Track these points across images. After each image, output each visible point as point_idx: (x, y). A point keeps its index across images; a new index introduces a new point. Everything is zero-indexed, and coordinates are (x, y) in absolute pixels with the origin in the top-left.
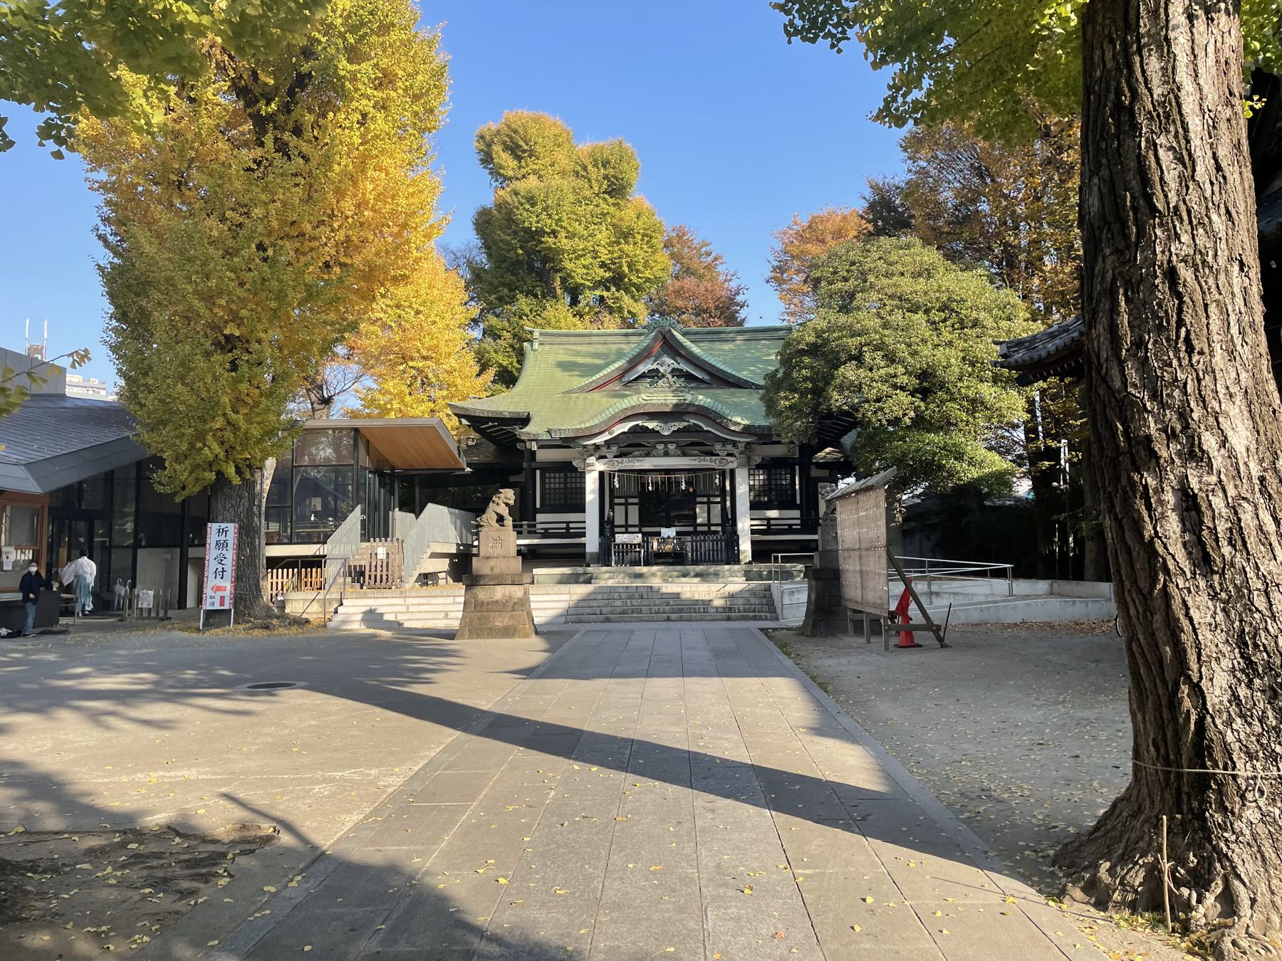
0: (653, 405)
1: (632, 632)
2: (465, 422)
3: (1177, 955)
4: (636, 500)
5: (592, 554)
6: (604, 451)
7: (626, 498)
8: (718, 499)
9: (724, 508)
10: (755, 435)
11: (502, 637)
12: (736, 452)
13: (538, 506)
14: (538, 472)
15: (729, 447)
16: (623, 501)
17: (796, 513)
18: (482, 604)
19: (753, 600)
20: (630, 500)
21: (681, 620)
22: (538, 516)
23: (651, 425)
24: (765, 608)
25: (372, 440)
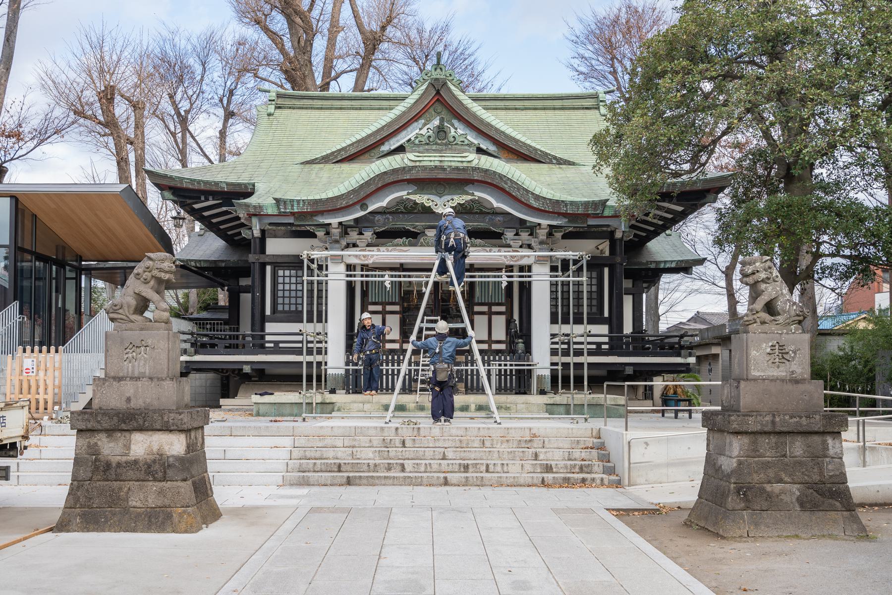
0: (425, 168)
1: (388, 513)
2: (167, 194)
3: (581, 534)
4: (397, 308)
5: (335, 377)
6: (353, 235)
7: (384, 304)
8: (503, 309)
9: (509, 322)
10: (564, 215)
11: (148, 529)
12: (533, 242)
13: (268, 312)
14: (268, 268)
15: (525, 235)
16: (379, 308)
17: (604, 329)
18: (108, 465)
19: (577, 454)
20: (389, 308)
21: (466, 483)
22: (270, 327)
23: (422, 199)
24: (598, 466)
25: (40, 215)
